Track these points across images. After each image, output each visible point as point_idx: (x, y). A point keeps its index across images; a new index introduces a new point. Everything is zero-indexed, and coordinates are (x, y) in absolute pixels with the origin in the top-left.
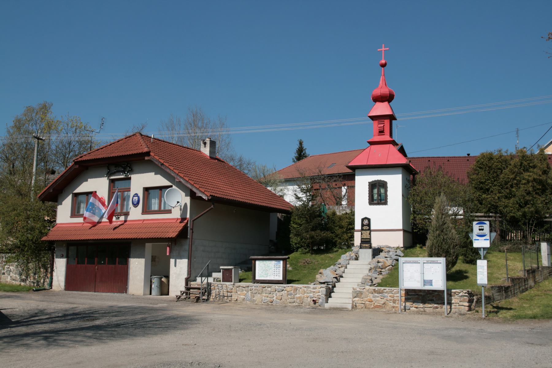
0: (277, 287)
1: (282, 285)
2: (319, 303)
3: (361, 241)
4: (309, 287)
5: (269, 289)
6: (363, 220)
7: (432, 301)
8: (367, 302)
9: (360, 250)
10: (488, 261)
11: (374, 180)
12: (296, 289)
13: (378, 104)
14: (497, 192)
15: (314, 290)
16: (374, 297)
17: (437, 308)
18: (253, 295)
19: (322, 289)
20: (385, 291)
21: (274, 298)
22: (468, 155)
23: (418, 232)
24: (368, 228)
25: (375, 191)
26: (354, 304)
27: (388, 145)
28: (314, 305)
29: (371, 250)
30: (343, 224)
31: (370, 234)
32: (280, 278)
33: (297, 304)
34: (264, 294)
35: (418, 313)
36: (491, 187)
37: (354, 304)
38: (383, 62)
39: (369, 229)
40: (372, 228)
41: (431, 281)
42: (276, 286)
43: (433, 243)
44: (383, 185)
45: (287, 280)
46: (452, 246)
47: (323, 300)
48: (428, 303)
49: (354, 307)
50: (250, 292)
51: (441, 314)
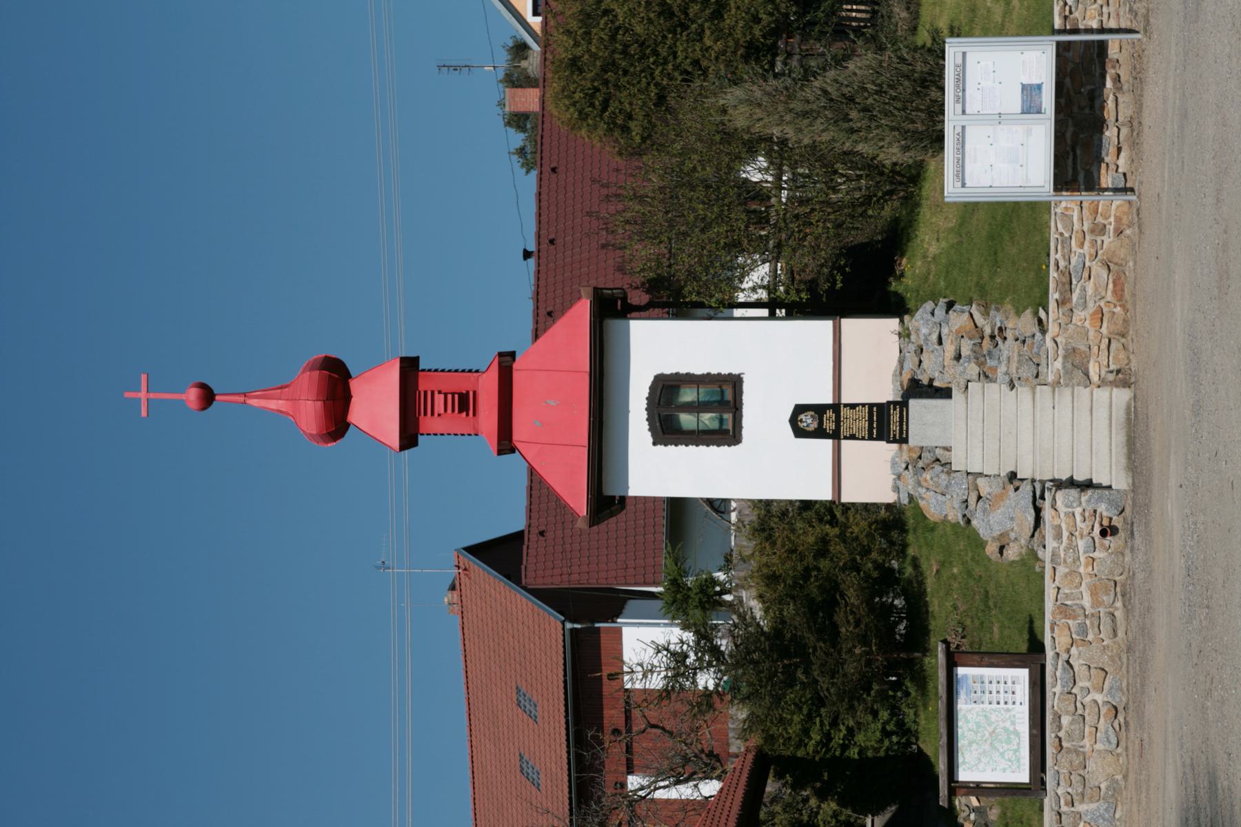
0: (1058, 689)
2: (1113, 513)
3: (879, 438)
5: (1065, 720)
6: (800, 433)
7: (1095, 98)
8: (1104, 330)
9: (912, 442)
10: (955, 32)
11: (646, 425)
12: (1064, 610)
13: (357, 415)
14: (698, 46)
15: (1065, 534)
17: (1117, 79)
18: (1087, 791)
19: (1059, 504)
20: (1062, 264)
21: (1100, 698)
22: (527, 255)
23: (844, 273)
24: (830, 413)
26: (1111, 377)
27: (516, 376)
28: (1122, 534)
29: (912, 402)
30: (811, 539)
31: (853, 406)
32: (1023, 674)
33: (1119, 604)
34: (1087, 742)
35: (1135, 144)
36: (676, 68)
37: (1111, 377)
38: (193, 394)
39: (836, 407)
41: (1024, 87)
42: (1055, 690)
43: (892, 129)
44: (666, 389)
45: (1031, 654)
46: (905, 68)
47: (1100, 499)
48: (1102, 108)
49: (1122, 378)
50: (1080, 808)
51: (1138, 57)
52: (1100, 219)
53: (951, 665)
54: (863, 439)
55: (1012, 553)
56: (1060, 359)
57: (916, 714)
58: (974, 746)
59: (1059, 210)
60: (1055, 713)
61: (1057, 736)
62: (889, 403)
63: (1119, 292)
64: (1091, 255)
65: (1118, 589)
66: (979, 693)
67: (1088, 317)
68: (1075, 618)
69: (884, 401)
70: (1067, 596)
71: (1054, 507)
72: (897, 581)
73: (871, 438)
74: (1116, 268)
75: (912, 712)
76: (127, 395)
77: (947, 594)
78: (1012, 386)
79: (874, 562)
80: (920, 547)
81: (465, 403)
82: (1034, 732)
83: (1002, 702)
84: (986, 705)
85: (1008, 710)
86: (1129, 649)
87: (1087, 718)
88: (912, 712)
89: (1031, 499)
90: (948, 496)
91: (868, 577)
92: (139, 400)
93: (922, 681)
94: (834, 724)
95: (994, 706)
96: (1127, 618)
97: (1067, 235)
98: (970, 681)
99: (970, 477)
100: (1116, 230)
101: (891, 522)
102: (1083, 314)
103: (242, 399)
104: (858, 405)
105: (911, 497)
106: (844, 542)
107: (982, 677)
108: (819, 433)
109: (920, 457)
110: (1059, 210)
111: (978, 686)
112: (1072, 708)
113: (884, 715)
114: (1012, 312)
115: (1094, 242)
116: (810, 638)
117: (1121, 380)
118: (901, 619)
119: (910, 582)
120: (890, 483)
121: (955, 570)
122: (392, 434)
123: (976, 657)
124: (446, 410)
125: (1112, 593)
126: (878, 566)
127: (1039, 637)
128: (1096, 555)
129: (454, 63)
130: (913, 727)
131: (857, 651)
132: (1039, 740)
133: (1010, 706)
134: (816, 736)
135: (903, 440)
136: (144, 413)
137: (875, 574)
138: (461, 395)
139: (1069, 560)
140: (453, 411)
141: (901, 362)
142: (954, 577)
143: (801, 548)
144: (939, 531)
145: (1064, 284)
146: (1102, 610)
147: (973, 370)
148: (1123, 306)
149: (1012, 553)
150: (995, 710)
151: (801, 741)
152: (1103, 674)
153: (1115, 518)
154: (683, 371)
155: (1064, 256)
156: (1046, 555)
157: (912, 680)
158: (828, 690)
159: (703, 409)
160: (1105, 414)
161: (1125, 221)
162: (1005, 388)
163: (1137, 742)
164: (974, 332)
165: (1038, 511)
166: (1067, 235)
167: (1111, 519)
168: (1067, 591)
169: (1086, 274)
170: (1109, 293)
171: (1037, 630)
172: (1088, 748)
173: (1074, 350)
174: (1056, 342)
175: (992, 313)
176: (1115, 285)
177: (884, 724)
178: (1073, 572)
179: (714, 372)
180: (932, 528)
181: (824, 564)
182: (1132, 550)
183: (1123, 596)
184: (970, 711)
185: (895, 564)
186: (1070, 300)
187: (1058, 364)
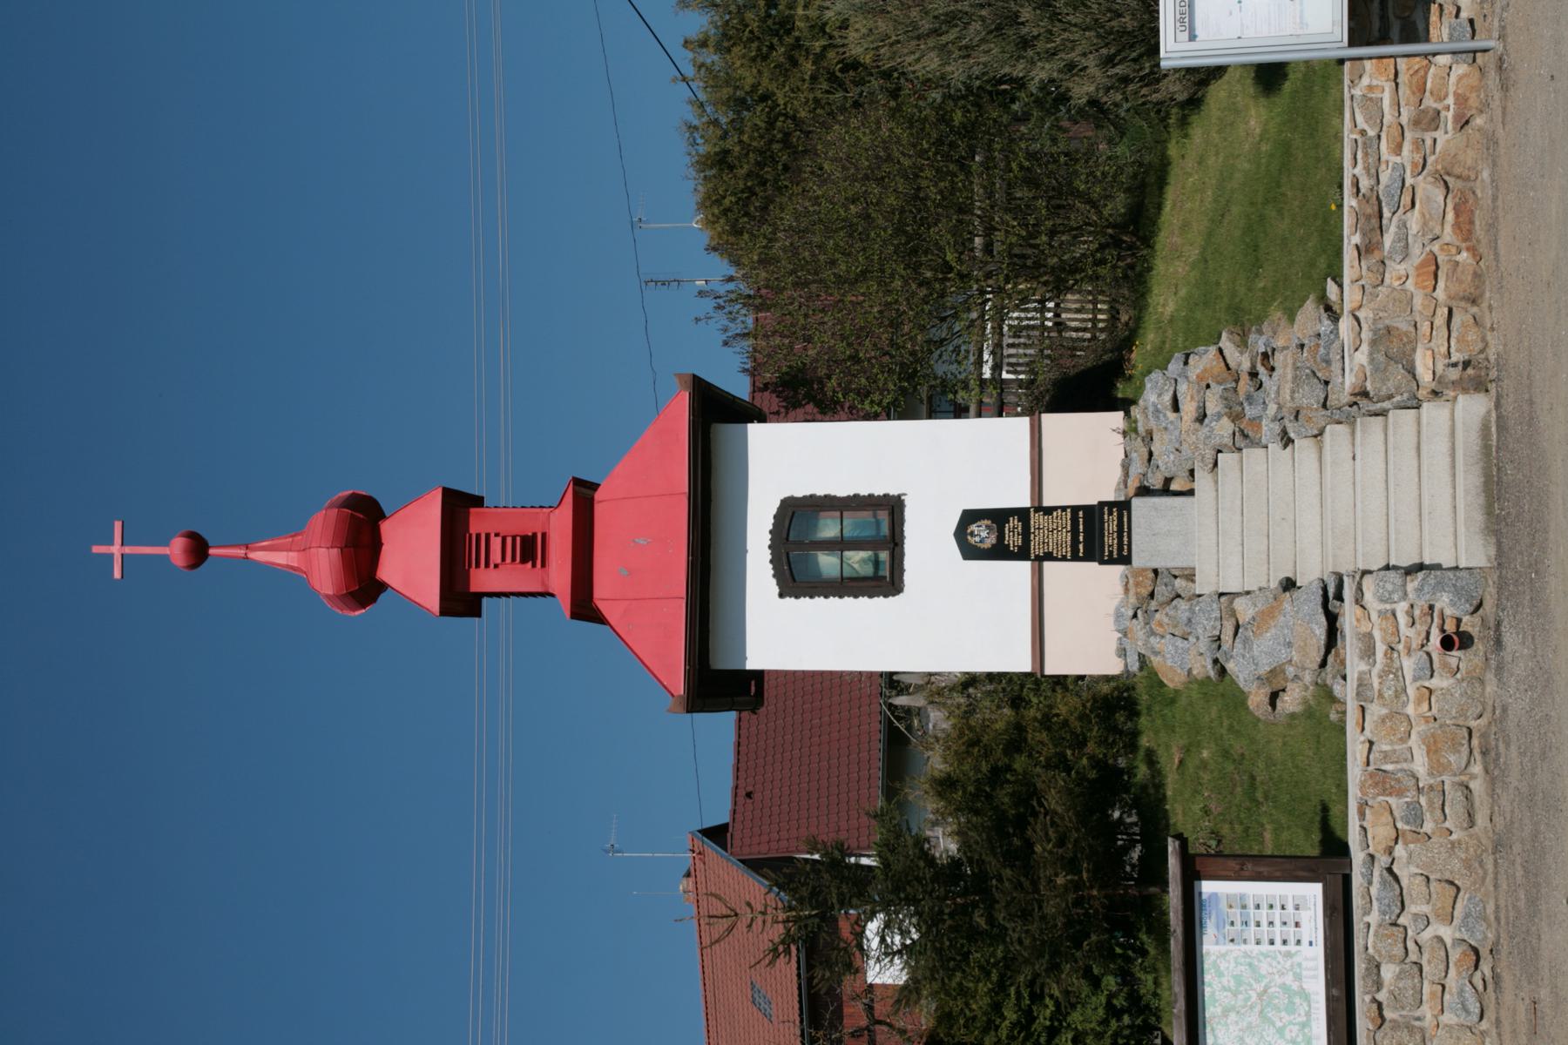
0: (1374, 918)
1: (1357, 881)
3: (1088, 557)
4: (1363, 684)
5: (1388, 972)
6: (970, 552)
8: (1440, 293)
9: (1137, 561)
11: (769, 570)
12: (1381, 781)
13: (388, 571)
15: (1380, 649)
16: (1406, 256)
19: (1368, 597)
20: (1365, 184)
21: (1447, 933)
24: (1014, 522)
25: (828, 563)
26: (1454, 374)
28: (1479, 647)
31: (1049, 511)
32: (1313, 892)
33: (1477, 768)
34: (1427, 1011)
37: (1454, 374)
38: (176, 549)
39: (1023, 514)
40: (1021, 498)
42: (1368, 919)
44: (796, 517)
45: (1326, 858)
47: (1440, 586)
49: (1474, 375)
52: (1429, 102)
53: (1191, 875)
54: (1064, 559)
55: (1290, 702)
56: (1365, 348)
57: (1156, 983)
58: (1233, 1016)
59: (1357, 92)
60: (1370, 960)
61: (1374, 1000)
62: (1102, 504)
63: (1464, 227)
64: (1414, 164)
65: (1475, 742)
66: (1238, 926)
67: (1412, 272)
68: (1400, 793)
69: (1092, 500)
70: (1386, 756)
71: (1359, 600)
72: (1126, 788)
73: (1075, 558)
74: (1460, 184)
75: (1150, 978)
76: (96, 549)
77: (1196, 792)
78: (1287, 441)
79: (1091, 757)
80: (1157, 732)
81: (530, 549)
82: (1335, 992)
83: (1278, 941)
84: (1251, 947)
85: (1288, 955)
86: (1498, 846)
87: (1426, 969)
88: (1150, 978)
89: (1319, 600)
90: (1192, 639)
91: (1082, 778)
92: (112, 555)
93: (1161, 932)
94: (1037, 997)
95: (1265, 947)
96: (1492, 793)
97: (1371, 133)
98: (1223, 905)
99: (1223, 599)
100: (1457, 118)
101: (1115, 705)
102: (1401, 268)
103: (241, 552)
104: (1056, 508)
105: (1142, 658)
106: (1049, 729)
107: (1242, 897)
108: (1000, 552)
109: (1152, 595)
110: (1357, 92)
111: (1236, 914)
112: (1398, 951)
113: (1110, 982)
114: (1284, 322)
115: (1419, 144)
116: (993, 864)
117: (1471, 379)
118: (1131, 844)
119: (1144, 788)
120: (1114, 645)
121: (1205, 754)
122: (428, 591)
123: (1232, 864)
124: (503, 559)
125: (1465, 750)
126: (1096, 763)
127: (1339, 833)
128: (1434, 683)
129: (662, 278)
130: (1154, 1003)
131: (1060, 881)
132: (1343, 1007)
133: (1292, 947)
134: (1011, 1015)
135: (1125, 560)
136: (117, 575)
137: (1093, 775)
138: (525, 539)
139: (1388, 693)
140: (514, 559)
141: (1126, 467)
142: (1204, 765)
143: (985, 739)
144: (1183, 701)
145: (1368, 218)
146: (1447, 779)
147: (1223, 429)
148: (1472, 250)
149: (1290, 702)
150: (1266, 956)
151: (990, 1021)
152: (1453, 891)
153: (1466, 619)
154: (820, 492)
155: (1367, 169)
156: (1347, 691)
157: (1149, 932)
158: (1020, 942)
159: (850, 547)
160: (1443, 446)
161: (1473, 101)
162: (1276, 448)
163: (1522, 1008)
164: (1226, 374)
165: (1332, 619)
166: (1371, 133)
167: (1459, 621)
168: (1386, 748)
169: (1406, 199)
170: (1448, 229)
171: (1335, 823)
172: (1429, 1021)
173: (1389, 330)
174: (1357, 319)
175: (1252, 337)
176: (1457, 215)
177: (1111, 996)
178: (1396, 715)
179: (864, 492)
180: (1172, 700)
181: (1020, 762)
182: (1500, 669)
183: (1484, 753)
184: (1223, 956)
185: (1122, 762)
186: (1380, 245)
187: (1362, 357)
